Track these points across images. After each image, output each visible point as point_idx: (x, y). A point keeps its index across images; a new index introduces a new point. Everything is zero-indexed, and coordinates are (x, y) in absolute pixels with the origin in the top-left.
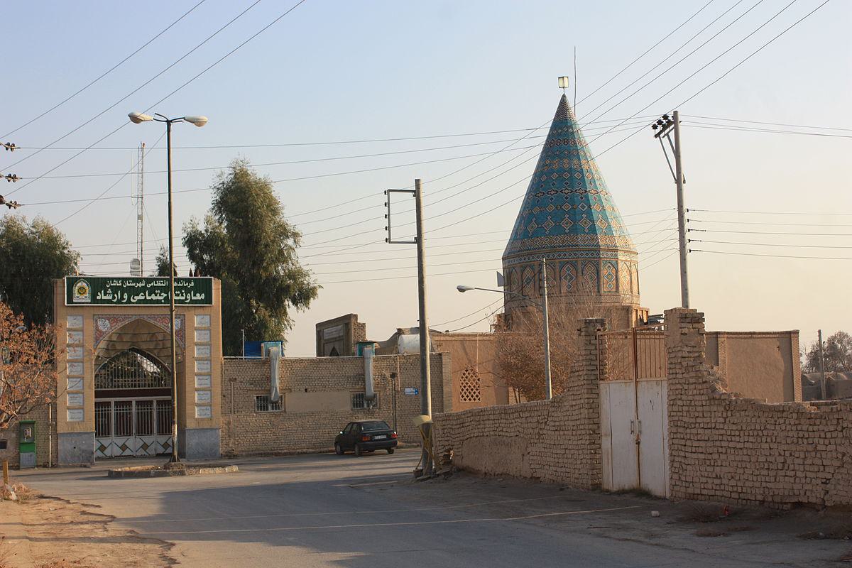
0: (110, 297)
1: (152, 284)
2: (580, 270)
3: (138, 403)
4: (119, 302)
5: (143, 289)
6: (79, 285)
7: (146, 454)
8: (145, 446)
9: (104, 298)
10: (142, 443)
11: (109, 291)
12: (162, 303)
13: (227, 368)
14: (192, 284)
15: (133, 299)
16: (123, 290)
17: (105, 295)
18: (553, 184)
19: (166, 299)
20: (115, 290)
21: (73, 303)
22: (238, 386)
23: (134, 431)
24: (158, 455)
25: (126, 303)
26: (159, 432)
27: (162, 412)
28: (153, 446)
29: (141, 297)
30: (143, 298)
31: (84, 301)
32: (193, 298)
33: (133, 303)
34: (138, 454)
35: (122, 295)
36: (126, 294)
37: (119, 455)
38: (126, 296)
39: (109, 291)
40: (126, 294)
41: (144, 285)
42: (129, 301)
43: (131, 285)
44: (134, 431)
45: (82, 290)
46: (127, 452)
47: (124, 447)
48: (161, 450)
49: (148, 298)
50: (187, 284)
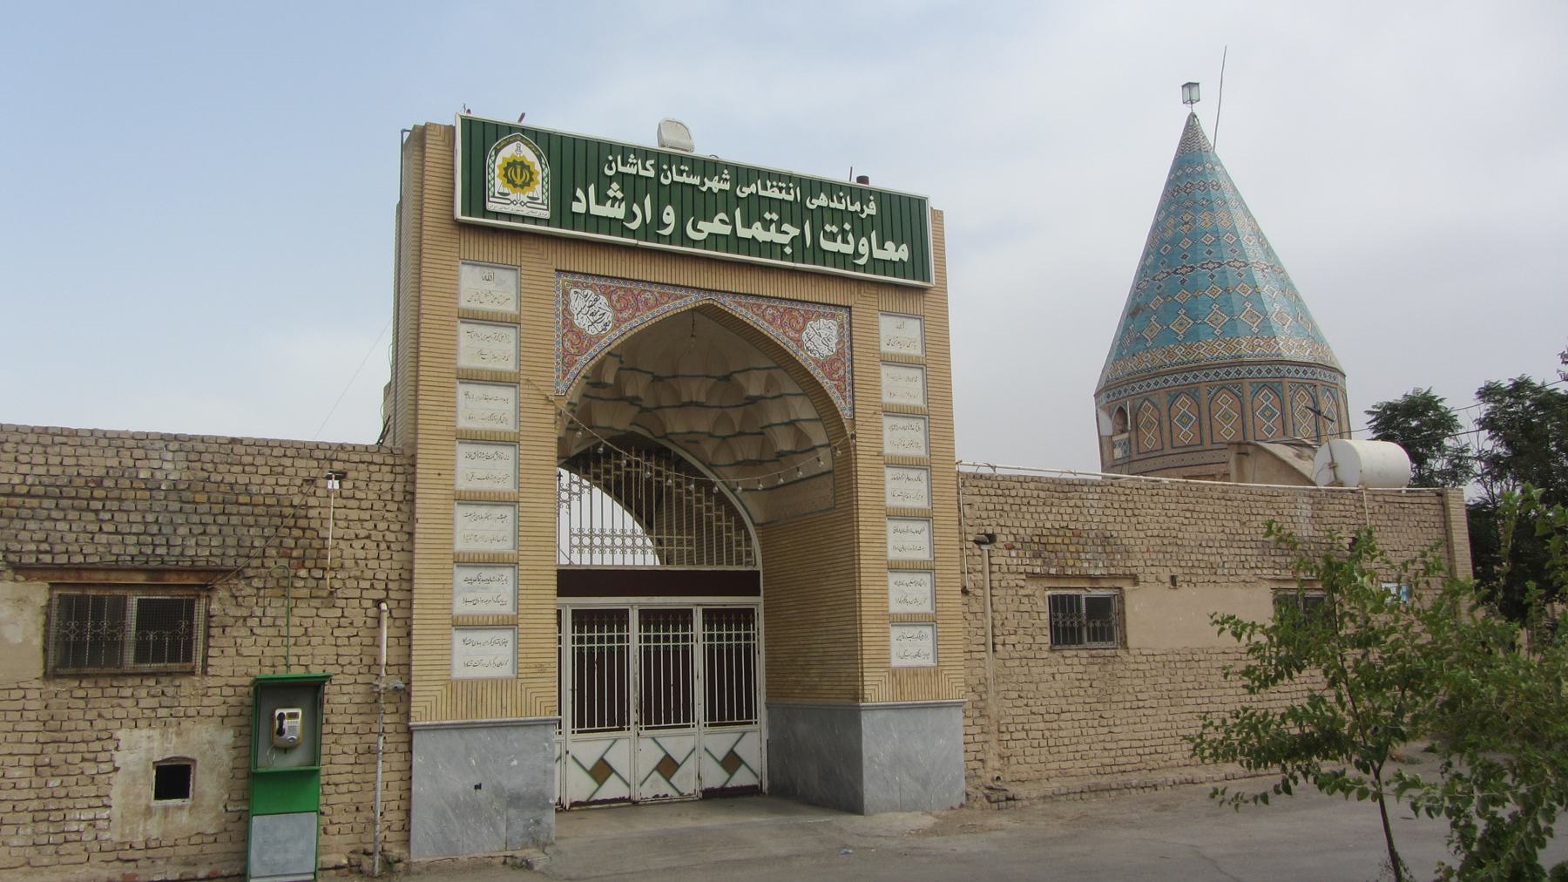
0: (618, 212)
1: (753, 189)
2: (1288, 399)
3: (647, 617)
4: (647, 231)
5: (727, 202)
6: (508, 152)
7: (671, 792)
8: (668, 766)
9: (596, 210)
10: (678, 759)
11: (615, 190)
12: (783, 256)
13: (969, 499)
14: (871, 209)
15: (694, 228)
16: (663, 195)
17: (623, 164)
18: (1210, 252)
19: (797, 242)
20: (634, 188)
21: (486, 213)
22: (1002, 561)
23: (634, 717)
24: (712, 796)
25: (670, 239)
26: (712, 717)
27: (657, 649)
28: (689, 768)
29: (717, 227)
30: (727, 230)
31: (525, 211)
32: (878, 254)
33: (694, 243)
34: (647, 792)
35: (658, 213)
36: (669, 209)
37: (583, 798)
38: (669, 215)
39: (615, 190)
40: (669, 209)
41: (727, 186)
42: (681, 236)
43: (684, 179)
44: (634, 717)
45: (517, 173)
46: (613, 788)
47: (601, 771)
48: (716, 777)
49: (743, 232)
50: (857, 207)
